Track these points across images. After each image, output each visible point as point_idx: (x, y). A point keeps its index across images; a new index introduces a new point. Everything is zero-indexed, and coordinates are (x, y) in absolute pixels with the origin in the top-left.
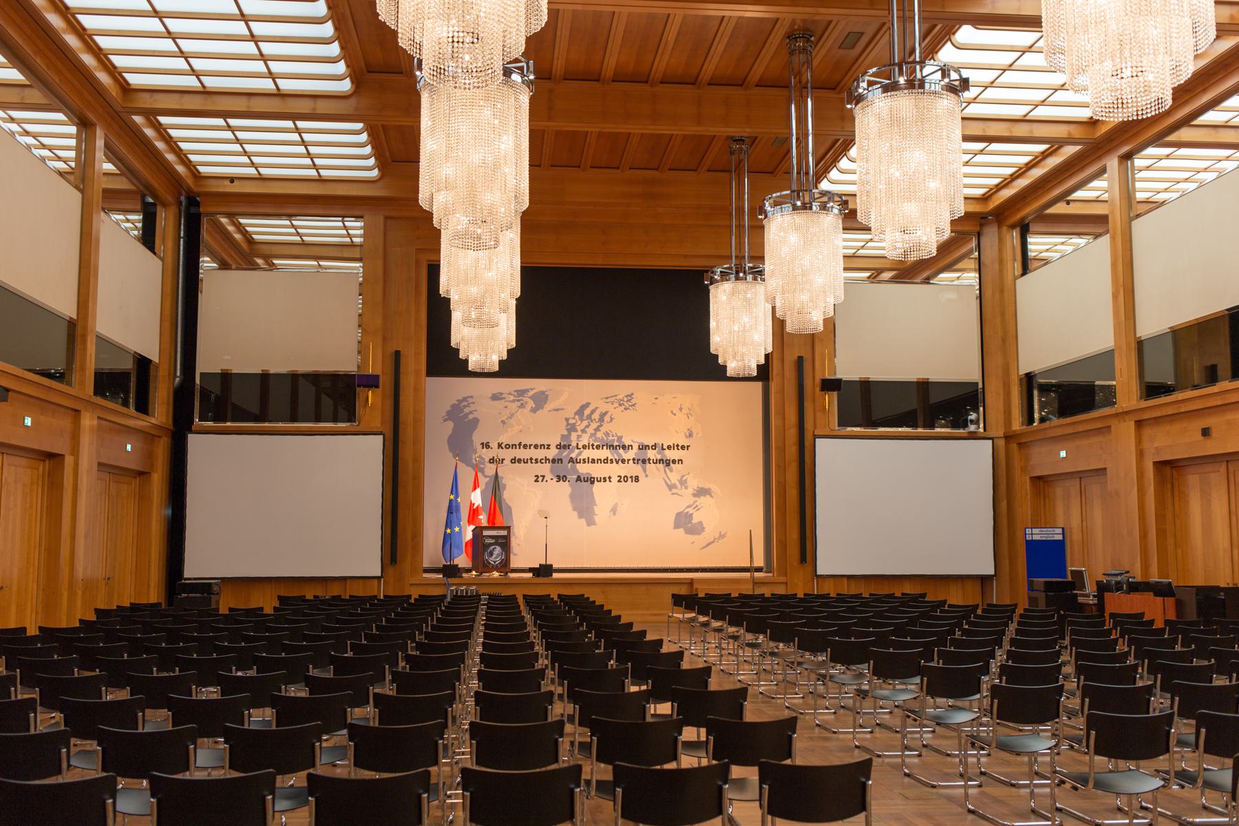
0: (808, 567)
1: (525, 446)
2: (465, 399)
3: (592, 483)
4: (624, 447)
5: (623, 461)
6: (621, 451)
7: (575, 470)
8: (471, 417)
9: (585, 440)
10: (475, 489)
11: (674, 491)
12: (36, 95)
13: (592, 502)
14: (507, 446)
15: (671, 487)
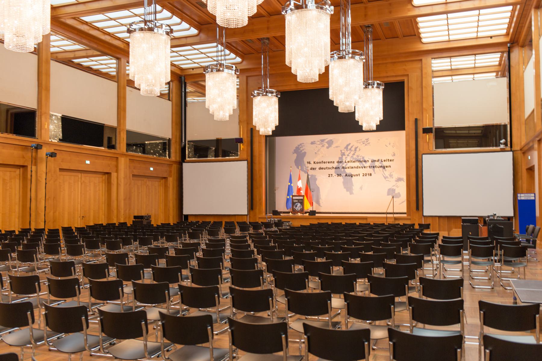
0: (420, 212)
1: (324, 163)
2: (301, 144)
3: (352, 177)
4: (365, 161)
5: (365, 167)
6: (364, 163)
7: (345, 172)
8: (303, 151)
9: (348, 159)
10: (299, 180)
11: (387, 179)
12: (91, 52)
13: (352, 184)
14: (317, 163)
15: (385, 178)
